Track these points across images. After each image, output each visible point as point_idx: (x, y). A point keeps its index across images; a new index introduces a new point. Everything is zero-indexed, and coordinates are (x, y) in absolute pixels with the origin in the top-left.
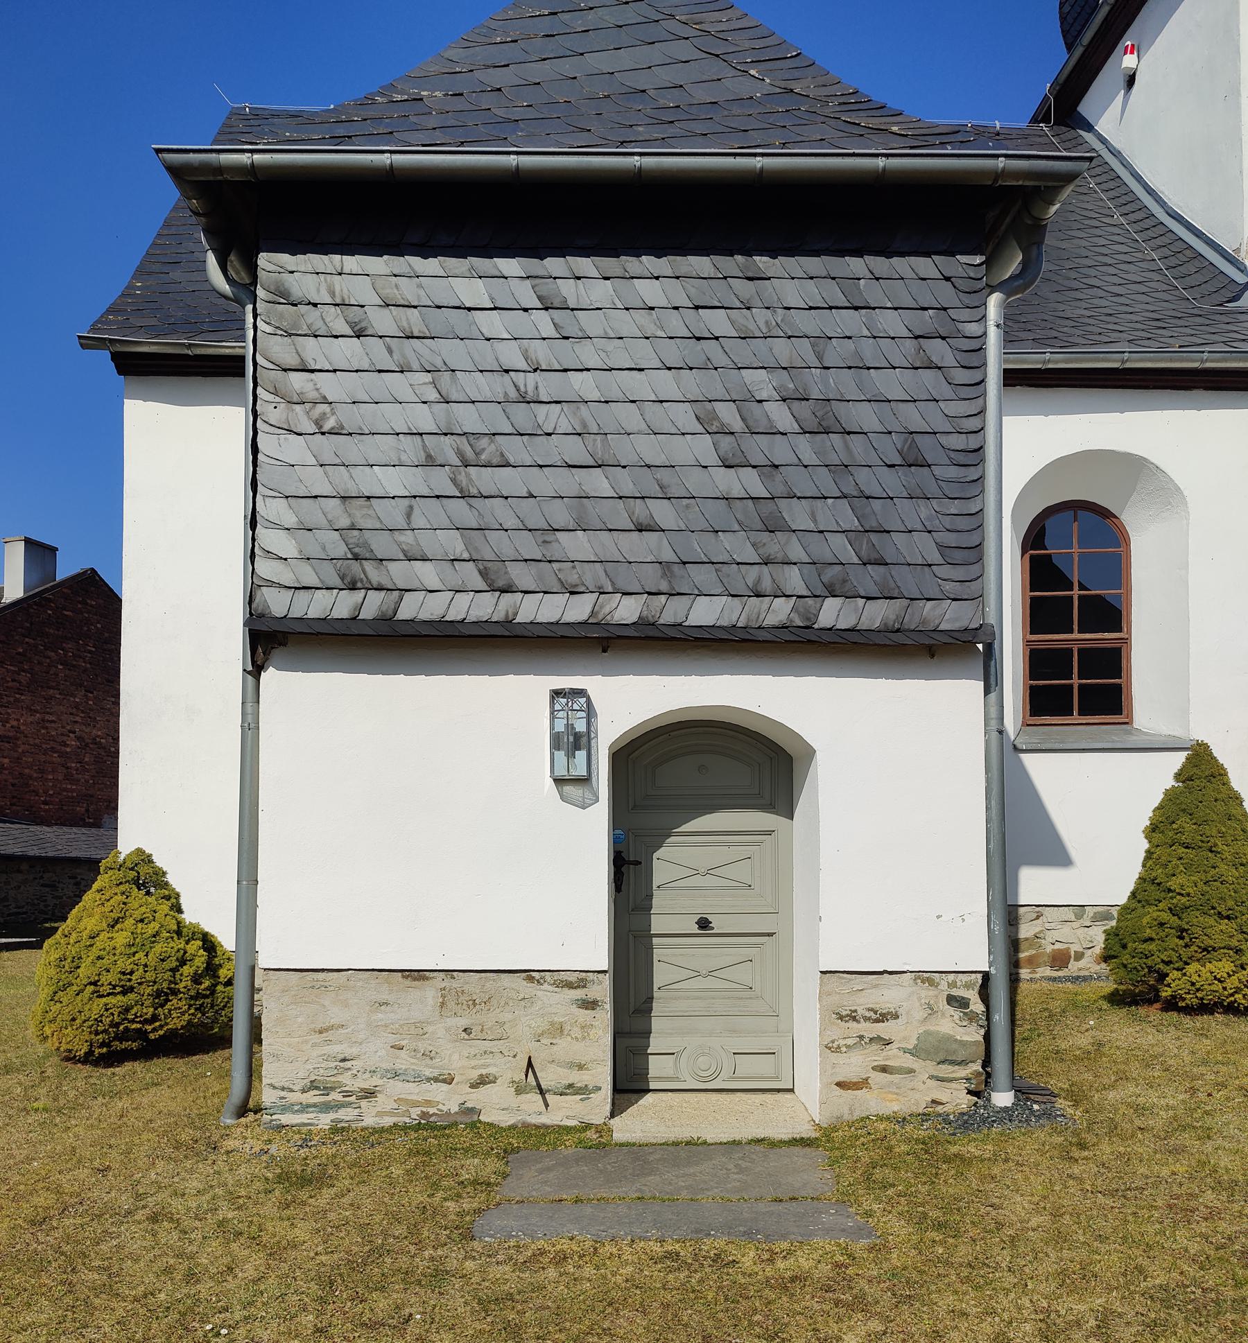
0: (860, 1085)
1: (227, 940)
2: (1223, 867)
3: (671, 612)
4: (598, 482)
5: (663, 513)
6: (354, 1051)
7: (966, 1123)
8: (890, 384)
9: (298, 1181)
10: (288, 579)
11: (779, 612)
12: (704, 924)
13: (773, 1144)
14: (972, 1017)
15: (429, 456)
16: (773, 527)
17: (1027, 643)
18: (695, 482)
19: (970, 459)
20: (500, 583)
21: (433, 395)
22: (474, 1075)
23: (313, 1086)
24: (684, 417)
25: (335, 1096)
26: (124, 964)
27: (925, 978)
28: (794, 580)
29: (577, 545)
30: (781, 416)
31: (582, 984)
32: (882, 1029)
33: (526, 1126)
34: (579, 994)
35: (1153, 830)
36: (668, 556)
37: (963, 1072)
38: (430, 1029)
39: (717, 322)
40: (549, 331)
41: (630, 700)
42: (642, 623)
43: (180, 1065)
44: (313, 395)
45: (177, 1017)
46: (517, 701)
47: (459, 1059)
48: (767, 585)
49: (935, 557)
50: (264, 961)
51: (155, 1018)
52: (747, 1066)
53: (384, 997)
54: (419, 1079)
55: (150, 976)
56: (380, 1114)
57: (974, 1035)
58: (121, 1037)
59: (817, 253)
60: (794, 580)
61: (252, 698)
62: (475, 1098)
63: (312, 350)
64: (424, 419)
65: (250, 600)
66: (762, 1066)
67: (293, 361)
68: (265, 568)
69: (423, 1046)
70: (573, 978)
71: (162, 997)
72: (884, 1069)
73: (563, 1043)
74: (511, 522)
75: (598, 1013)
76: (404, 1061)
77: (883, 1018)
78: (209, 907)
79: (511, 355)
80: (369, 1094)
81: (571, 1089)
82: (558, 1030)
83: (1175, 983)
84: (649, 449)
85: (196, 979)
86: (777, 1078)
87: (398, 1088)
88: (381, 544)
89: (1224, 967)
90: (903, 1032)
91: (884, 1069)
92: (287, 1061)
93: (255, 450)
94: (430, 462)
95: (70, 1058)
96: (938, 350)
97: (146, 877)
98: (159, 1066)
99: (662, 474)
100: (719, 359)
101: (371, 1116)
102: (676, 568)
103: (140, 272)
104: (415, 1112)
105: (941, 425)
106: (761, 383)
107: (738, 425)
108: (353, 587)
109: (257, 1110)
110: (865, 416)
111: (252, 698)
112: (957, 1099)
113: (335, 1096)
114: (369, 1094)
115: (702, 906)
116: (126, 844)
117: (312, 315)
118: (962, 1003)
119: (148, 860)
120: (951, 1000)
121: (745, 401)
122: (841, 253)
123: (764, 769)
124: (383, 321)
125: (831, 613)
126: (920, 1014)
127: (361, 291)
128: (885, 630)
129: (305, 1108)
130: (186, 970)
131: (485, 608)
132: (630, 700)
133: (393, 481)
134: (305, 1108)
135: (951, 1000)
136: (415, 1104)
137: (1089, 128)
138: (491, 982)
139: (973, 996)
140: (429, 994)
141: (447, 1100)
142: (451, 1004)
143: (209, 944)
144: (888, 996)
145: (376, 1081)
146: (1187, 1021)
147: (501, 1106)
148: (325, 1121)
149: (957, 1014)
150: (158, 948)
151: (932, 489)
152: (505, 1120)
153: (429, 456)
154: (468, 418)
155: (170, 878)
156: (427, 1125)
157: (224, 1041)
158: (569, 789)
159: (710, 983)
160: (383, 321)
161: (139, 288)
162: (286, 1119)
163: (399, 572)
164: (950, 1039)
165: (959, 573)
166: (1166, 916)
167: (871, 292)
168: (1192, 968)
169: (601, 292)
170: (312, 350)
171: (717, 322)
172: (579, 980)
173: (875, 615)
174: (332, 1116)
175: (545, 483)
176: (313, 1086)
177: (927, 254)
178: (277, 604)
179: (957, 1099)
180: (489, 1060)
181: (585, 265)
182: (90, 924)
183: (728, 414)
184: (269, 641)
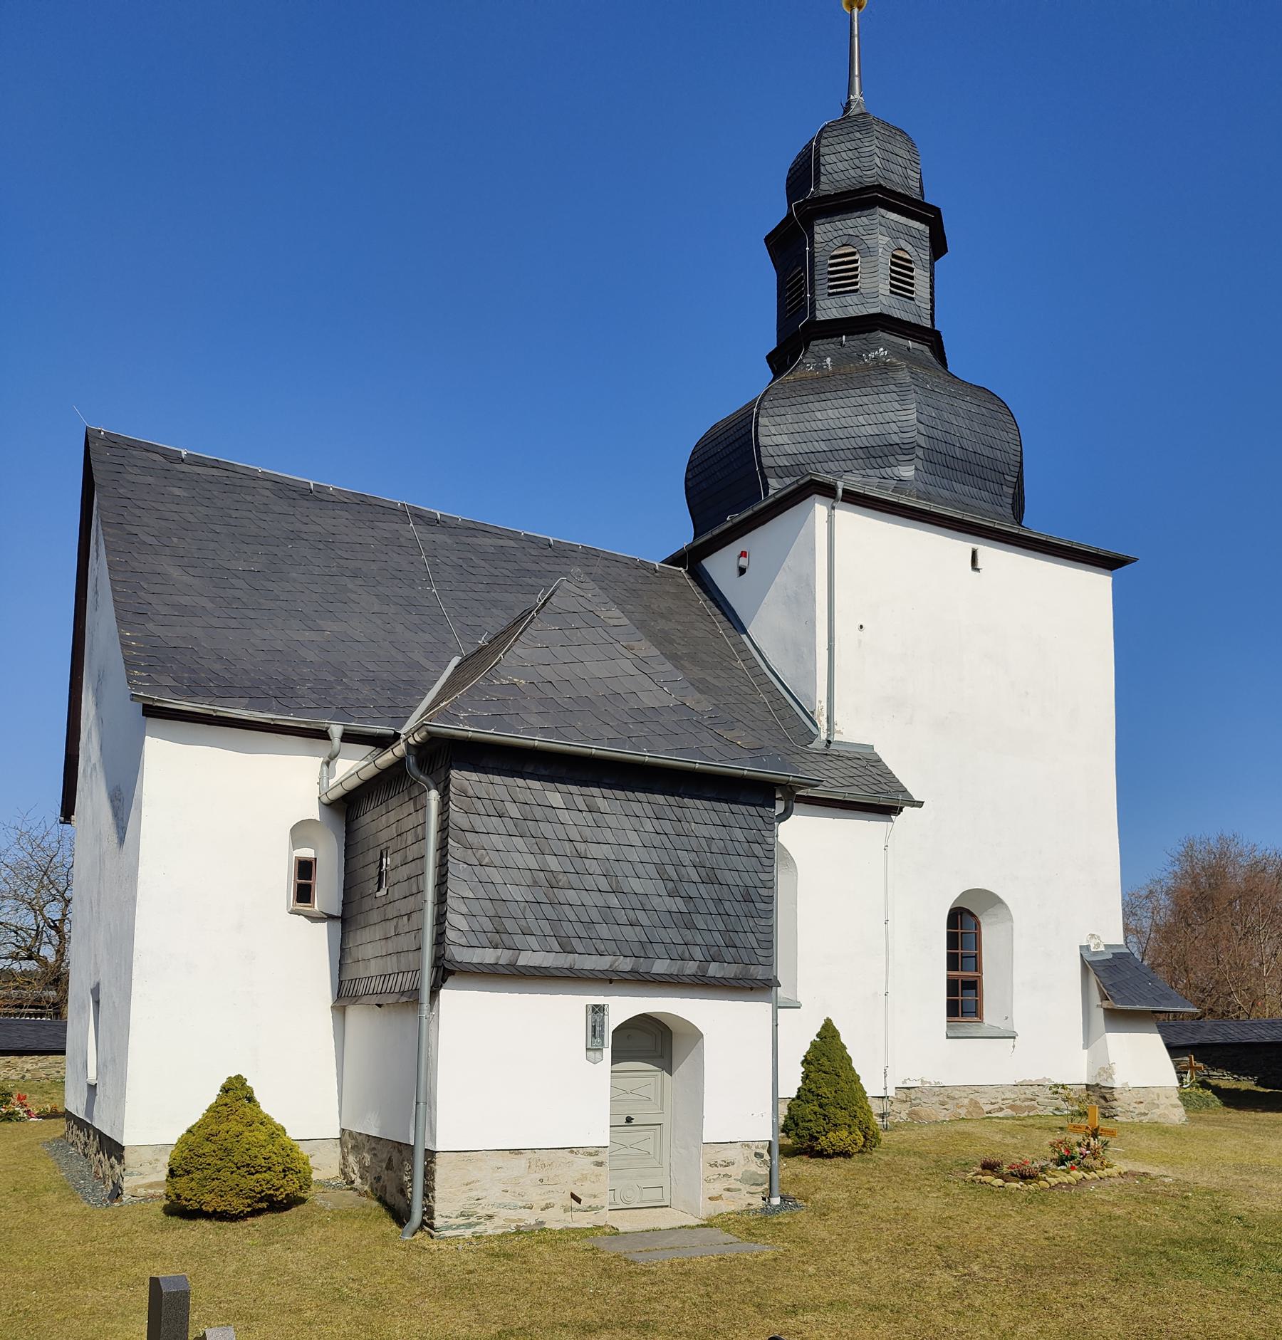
2: (842, 1084)
3: (643, 966)
4: (614, 901)
5: (642, 917)
6: (484, 1194)
7: (768, 1211)
8: (737, 862)
10: (463, 941)
11: (691, 968)
14: (764, 1162)
15: (535, 881)
16: (690, 926)
18: (656, 901)
20: (569, 949)
22: (543, 1204)
24: (651, 870)
25: (473, 1219)
27: (746, 1144)
28: (697, 953)
29: (603, 931)
31: (596, 1153)
32: (728, 1170)
33: (567, 1229)
35: (806, 1062)
36: (645, 939)
37: (760, 1189)
38: (522, 1180)
39: (667, 826)
40: (592, 823)
41: (623, 1007)
42: (633, 971)
46: (565, 1011)
47: (536, 1196)
49: (755, 945)
53: (499, 1165)
56: (496, 1228)
58: (261, 1200)
59: (709, 799)
60: (697, 953)
62: (543, 1216)
63: (478, 823)
64: (532, 862)
69: (518, 1190)
70: (592, 1151)
73: (587, 1184)
76: (507, 1199)
79: (574, 834)
80: (490, 1217)
82: (584, 1178)
83: (823, 1142)
84: (636, 885)
86: (663, 1200)
87: (505, 1213)
88: (510, 925)
94: (535, 884)
96: (757, 849)
100: (668, 845)
101: (490, 1229)
102: (649, 945)
106: (686, 857)
107: (675, 877)
110: (730, 878)
112: (758, 1202)
113: (473, 1219)
117: (478, 804)
120: (757, 1155)
121: (679, 865)
122: (719, 800)
124: (513, 810)
125: (714, 970)
126: (743, 1162)
127: (501, 792)
129: (458, 1227)
131: (564, 961)
132: (623, 1007)
133: (517, 893)
134: (458, 1227)
135: (757, 1155)
136: (514, 1221)
137: (745, 632)
139: (765, 1152)
140: (522, 1161)
141: (529, 1218)
142: (533, 1167)
146: (827, 1161)
147: (556, 1220)
148: (468, 1233)
149: (759, 1161)
152: (558, 1226)
153: (535, 881)
158: (591, 1053)
160: (513, 810)
162: (448, 1233)
163: (518, 940)
164: (755, 1173)
166: (817, 1109)
167: (731, 820)
168: (830, 1135)
170: (478, 823)
171: (667, 826)
172: (593, 1152)
173: (730, 971)
174: (472, 1230)
175: (588, 899)
179: (758, 1202)
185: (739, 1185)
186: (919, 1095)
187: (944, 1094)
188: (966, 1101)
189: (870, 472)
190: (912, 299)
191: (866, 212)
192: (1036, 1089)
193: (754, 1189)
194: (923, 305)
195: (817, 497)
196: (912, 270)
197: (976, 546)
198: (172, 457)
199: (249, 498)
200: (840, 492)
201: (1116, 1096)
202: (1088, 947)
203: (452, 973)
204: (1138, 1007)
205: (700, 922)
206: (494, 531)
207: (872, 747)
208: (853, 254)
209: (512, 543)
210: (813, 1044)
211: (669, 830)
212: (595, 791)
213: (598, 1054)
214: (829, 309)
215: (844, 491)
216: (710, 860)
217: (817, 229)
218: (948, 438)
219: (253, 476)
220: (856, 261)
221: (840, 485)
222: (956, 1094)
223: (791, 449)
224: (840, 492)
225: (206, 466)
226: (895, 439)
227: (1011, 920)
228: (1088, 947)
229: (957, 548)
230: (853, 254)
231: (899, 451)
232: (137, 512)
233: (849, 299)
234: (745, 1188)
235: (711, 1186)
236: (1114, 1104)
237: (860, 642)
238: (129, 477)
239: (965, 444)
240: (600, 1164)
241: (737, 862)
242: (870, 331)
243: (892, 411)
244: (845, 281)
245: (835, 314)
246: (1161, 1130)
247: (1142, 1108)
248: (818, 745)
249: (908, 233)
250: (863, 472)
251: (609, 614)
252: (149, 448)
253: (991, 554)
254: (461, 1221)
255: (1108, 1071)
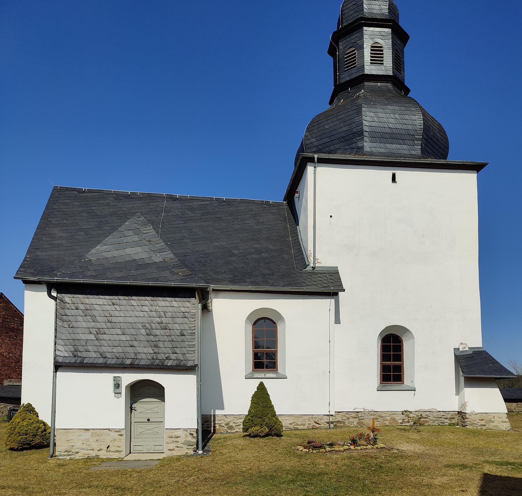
0: (173, 450)
1: (49, 424)
4: (123, 338)
6: (74, 444)
9: (60, 466)
12: (149, 420)
13: (153, 460)
14: (194, 437)
17: (253, 351)
19: (193, 335)
21: (92, 321)
22: (98, 449)
23: (66, 451)
26: (26, 429)
27: (185, 430)
30: (158, 326)
31: (120, 431)
32: (177, 439)
33: (108, 458)
34: (119, 433)
37: (192, 447)
41: (129, 378)
43: (38, 451)
44: (68, 320)
45: (37, 440)
46: (106, 379)
47: (95, 446)
48: (155, 357)
50: (56, 428)
51: (33, 440)
52: (157, 448)
54: (87, 450)
55: (32, 431)
57: (195, 440)
61: (55, 377)
65: (55, 359)
66: (160, 448)
67: (64, 314)
68: (58, 353)
69: (88, 443)
70: (118, 430)
71: (35, 435)
72: (177, 447)
73: (116, 442)
74: (106, 345)
75: (122, 437)
76: (84, 446)
77: (177, 437)
78: (44, 416)
80: (77, 453)
81: (117, 451)
85: (42, 432)
87: (83, 451)
88: (81, 348)
89: (257, 428)
90: (181, 440)
91: (177, 447)
92: (61, 447)
93: (56, 330)
94: (91, 333)
95: (12, 449)
97: (30, 409)
98: (33, 451)
99: (135, 336)
101: (77, 457)
103: (29, 252)
104: (86, 456)
105: (187, 328)
107: (150, 328)
108: (75, 357)
109: (55, 456)
111: (55, 377)
112: (191, 452)
114: (77, 453)
115: (148, 417)
116: (24, 401)
117: (68, 305)
118: (192, 434)
119: (31, 405)
123: (157, 392)
124: (82, 307)
126: (184, 437)
128: (177, 366)
129: (64, 455)
130: (40, 430)
132: (129, 378)
134: (64, 455)
135: (190, 434)
136: (86, 454)
138: (102, 431)
140: (89, 433)
141: (93, 454)
142: (94, 435)
143: (45, 424)
144: (178, 433)
145: (79, 450)
147: (103, 455)
148: (68, 458)
149: (191, 436)
150: (33, 425)
151: (185, 340)
154: (98, 325)
155: (36, 410)
156: (88, 458)
157: (48, 446)
158: (116, 395)
159: (150, 432)
160: (82, 307)
161: (28, 258)
162: (61, 458)
164: (190, 441)
165: (190, 355)
169: (124, 302)
176: (66, 451)
177: (185, 298)
178: (60, 360)
179: (191, 452)
180: (101, 446)
181: (121, 297)
182: (18, 420)
183: (148, 326)
184: (58, 367)
185: (182, 445)
186: (363, 415)
187: (376, 415)
188: (389, 418)
189: (347, 147)
190: (383, 64)
191: (359, 31)
192: (428, 413)
193: (189, 447)
194: (388, 65)
195: (308, 164)
196: (382, 51)
197: (394, 172)
198: (80, 191)
199: (102, 202)
200: (316, 160)
201: (467, 416)
202: (458, 349)
203: (61, 366)
204: (493, 376)
205: (161, 344)
206: (201, 199)
207: (337, 267)
208: (354, 50)
209: (208, 203)
210: (255, 392)
211: (148, 310)
212: (116, 297)
213: (119, 395)
214: (345, 77)
215: (318, 159)
216: (164, 320)
217: (340, 44)
218: (381, 125)
219: (109, 193)
220: (355, 53)
221: (316, 156)
222: (383, 415)
223: (316, 144)
224: (316, 160)
225: (92, 192)
226: (355, 130)
227: (414, 338)
228: (458, 349)
229: (386, 173)
230: (354, 50)
231: (357, 135)
232: (56, 213)
233: (353, 71)
234: (185, 447)
235: (169, 445)
236: (466, 420)
237: (330, 223)
238: (60, 201)
239: (391, 126)
240: (121, 435)
241: (179, 320)
242: (361, 83)
243: (376, 117)
244: (353, 60)
245: (348, 79)
246: (502, 434)
247: (483, 423)
248: (309, 269)
249: (381, 35)
250: (344, 148)
251: (145, 229)
252: (74, 190)
253: (402, 174)
254: (66, 453)
255: (464, 405)
